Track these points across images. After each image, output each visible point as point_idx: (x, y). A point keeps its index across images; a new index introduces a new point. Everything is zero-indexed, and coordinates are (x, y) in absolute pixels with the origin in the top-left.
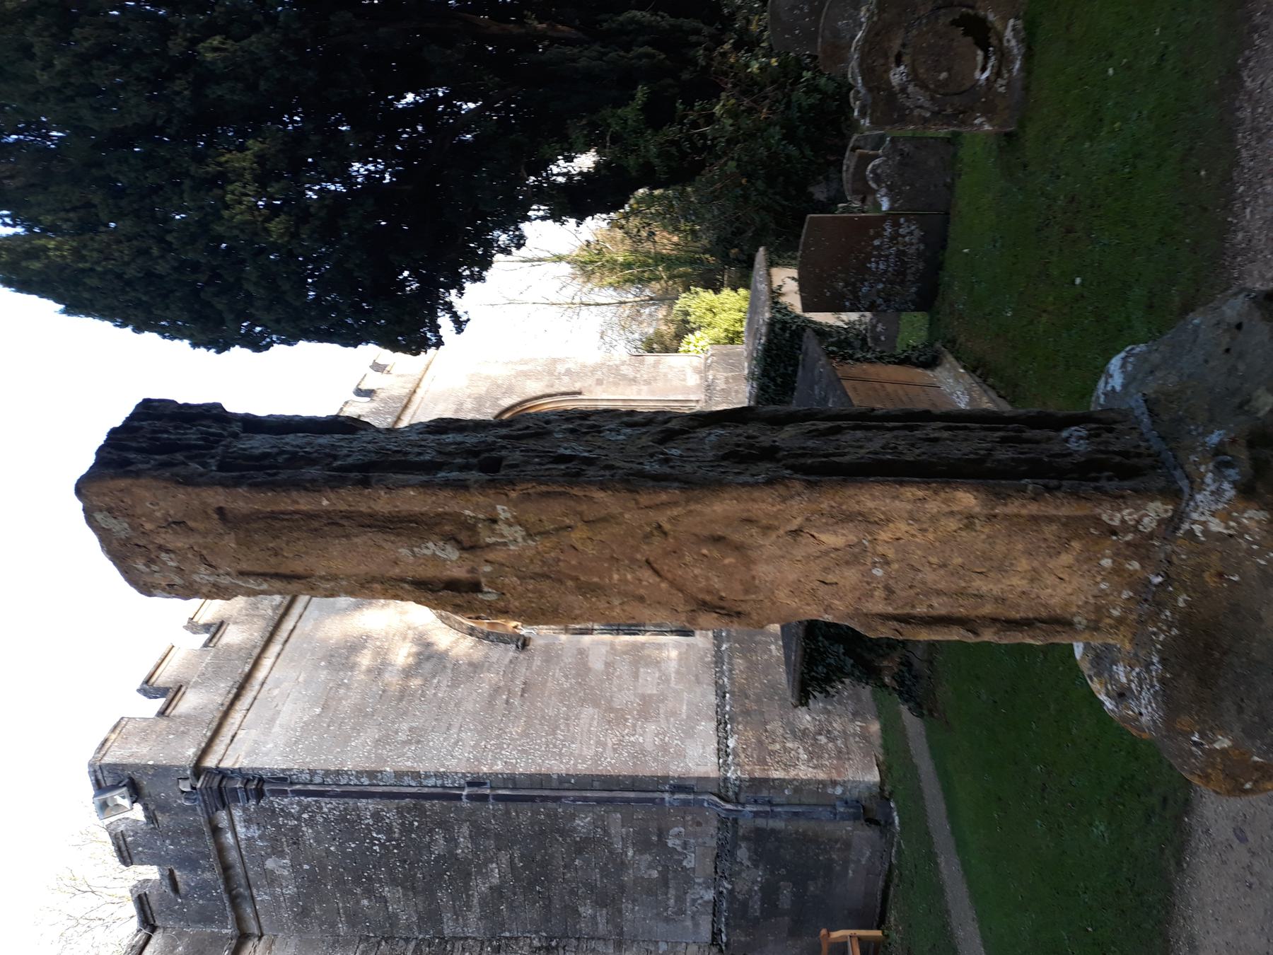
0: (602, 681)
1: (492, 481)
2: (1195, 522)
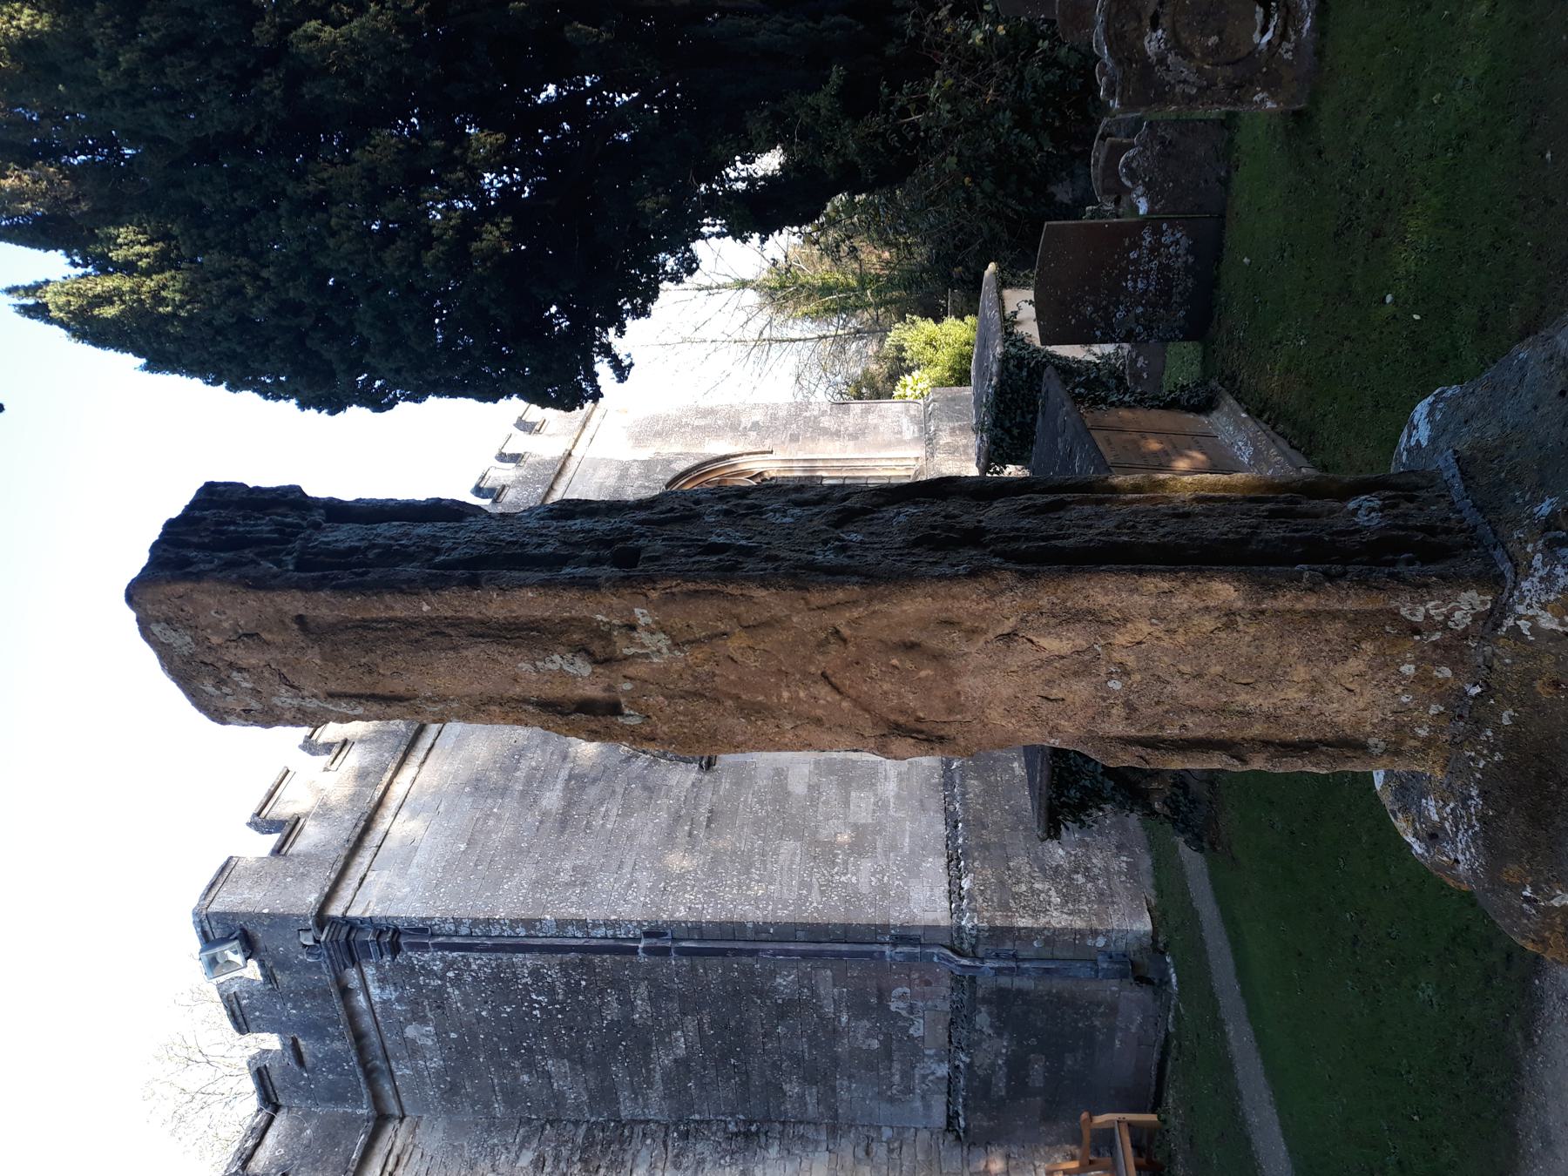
0: (805, 808)
1: (628, 578)
2: (1520, 617)
